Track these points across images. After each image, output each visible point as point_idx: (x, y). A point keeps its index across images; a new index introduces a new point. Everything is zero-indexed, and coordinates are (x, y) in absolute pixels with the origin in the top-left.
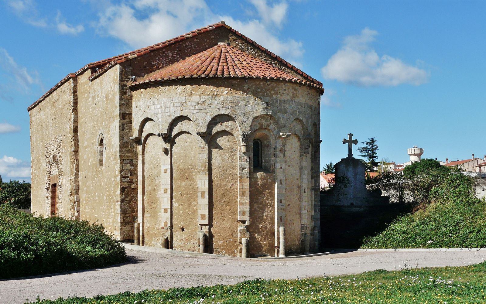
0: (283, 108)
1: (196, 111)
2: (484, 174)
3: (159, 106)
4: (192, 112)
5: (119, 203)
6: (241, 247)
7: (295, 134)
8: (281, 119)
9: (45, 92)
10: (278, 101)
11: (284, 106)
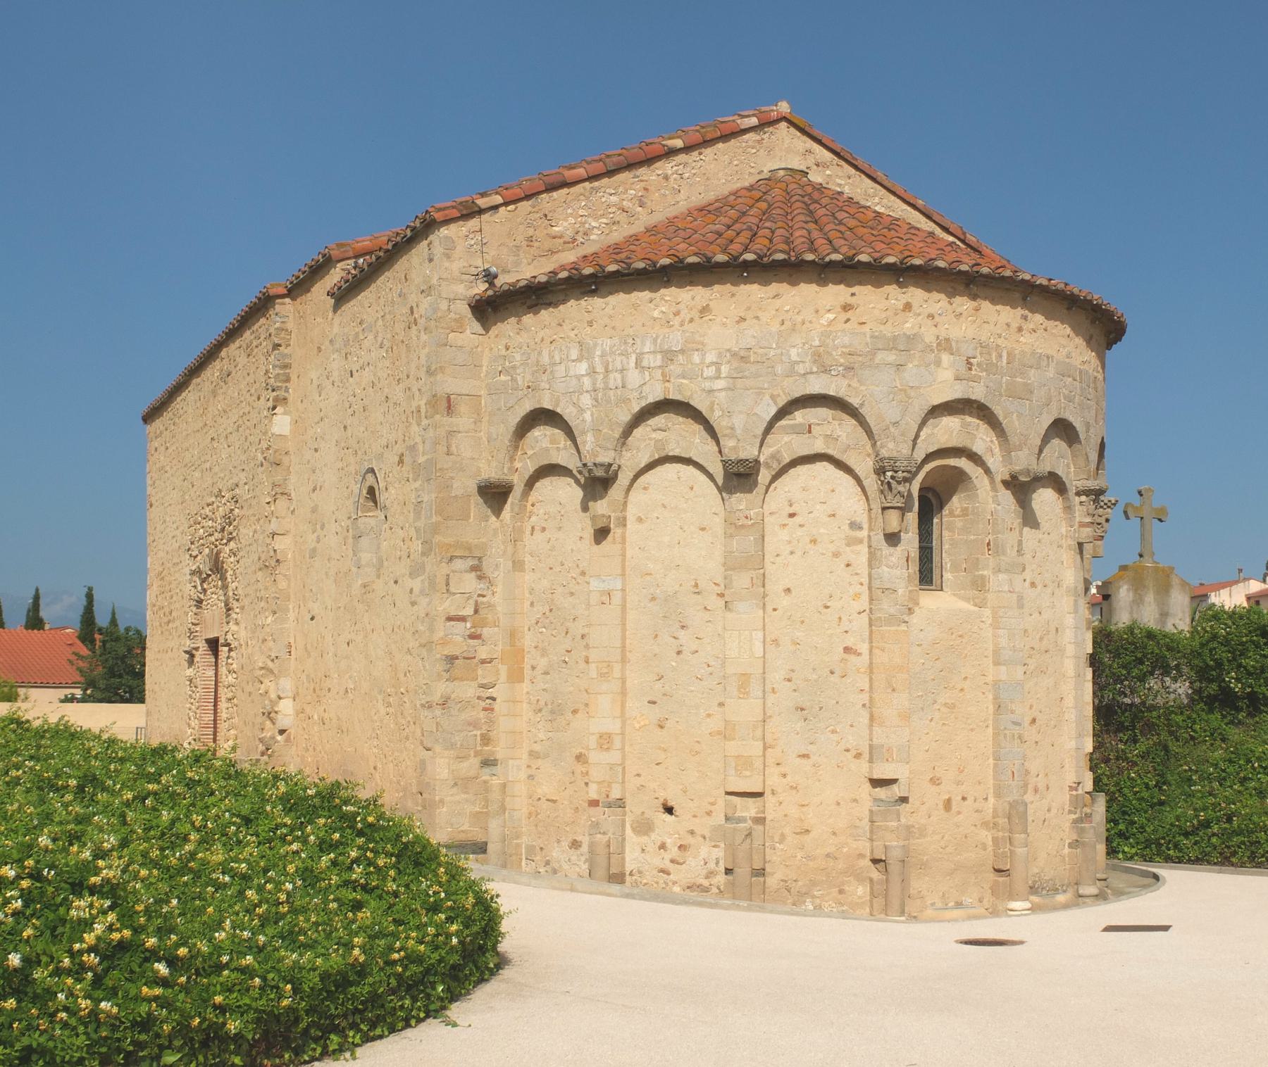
0: (1018, 379)
1: (720, 384)
2: (1267, 631)
3: (583, 368)
4: (707, 385)
9: (190, 359)
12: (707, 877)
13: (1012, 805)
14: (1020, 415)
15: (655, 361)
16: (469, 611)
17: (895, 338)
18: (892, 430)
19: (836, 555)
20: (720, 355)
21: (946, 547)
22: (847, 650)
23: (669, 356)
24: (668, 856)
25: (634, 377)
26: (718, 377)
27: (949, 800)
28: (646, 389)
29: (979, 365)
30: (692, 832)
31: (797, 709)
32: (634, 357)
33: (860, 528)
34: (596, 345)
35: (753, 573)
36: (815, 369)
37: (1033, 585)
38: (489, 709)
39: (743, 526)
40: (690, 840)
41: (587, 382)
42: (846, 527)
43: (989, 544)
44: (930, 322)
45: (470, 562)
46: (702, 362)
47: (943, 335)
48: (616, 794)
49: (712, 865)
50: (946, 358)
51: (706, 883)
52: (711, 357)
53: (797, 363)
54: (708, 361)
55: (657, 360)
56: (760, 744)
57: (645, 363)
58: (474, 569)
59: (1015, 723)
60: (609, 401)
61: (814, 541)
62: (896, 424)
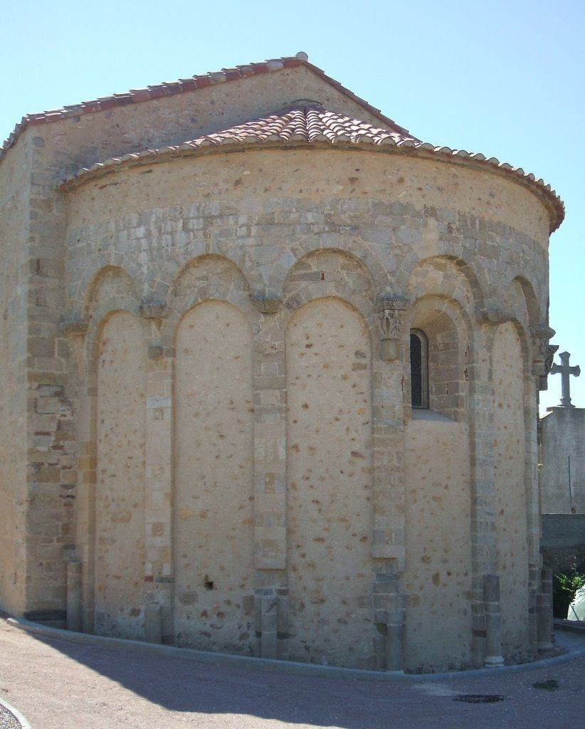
1: (251, 241)
3: (141, 232)
5: (25, 507)
6: (300, 601)
7: (514, 320)
8: (486, 271)
10: (477, 222)
11: (492, 239)
12: (240, 639)
13: (488, 578)
14: (490, 270)
15: (195, 224)
16: (53, 427)
17: (391, 205)
18: (389, 277)
19: (345, 378)
20: (250, 218)
21: (432, 375)
22: (354, 454)
23: (209, 220)
24: (208, 622)
25: (181, 237)
26: (249, 236)
27: (351, 192)
28: (191, 247)
29: (457, 229)
30: (228, 602)
31: (313, 501)
32: (181, 221)
33: (365, 357)
34: (151, 213)
35: (277, 393)
36: (327, 229)
37: (500, 405)
38: (68, 505)
39: (269, 355)
40: (224, 609)
41: (144, 242)
42: (353, 356)
43: (466, 372)
44: (418, 193)
46: (236, 223)
47: (429, 205)
48: (167, 571)
49: (244, 629)
50: (432, 222)
51: (239, 643)
52: (243, 219)
56: (284, 529)
57: (190, 226)
59: (489, 514)
60: (161, 257)
61: (326, 366)
62: (392, 273)
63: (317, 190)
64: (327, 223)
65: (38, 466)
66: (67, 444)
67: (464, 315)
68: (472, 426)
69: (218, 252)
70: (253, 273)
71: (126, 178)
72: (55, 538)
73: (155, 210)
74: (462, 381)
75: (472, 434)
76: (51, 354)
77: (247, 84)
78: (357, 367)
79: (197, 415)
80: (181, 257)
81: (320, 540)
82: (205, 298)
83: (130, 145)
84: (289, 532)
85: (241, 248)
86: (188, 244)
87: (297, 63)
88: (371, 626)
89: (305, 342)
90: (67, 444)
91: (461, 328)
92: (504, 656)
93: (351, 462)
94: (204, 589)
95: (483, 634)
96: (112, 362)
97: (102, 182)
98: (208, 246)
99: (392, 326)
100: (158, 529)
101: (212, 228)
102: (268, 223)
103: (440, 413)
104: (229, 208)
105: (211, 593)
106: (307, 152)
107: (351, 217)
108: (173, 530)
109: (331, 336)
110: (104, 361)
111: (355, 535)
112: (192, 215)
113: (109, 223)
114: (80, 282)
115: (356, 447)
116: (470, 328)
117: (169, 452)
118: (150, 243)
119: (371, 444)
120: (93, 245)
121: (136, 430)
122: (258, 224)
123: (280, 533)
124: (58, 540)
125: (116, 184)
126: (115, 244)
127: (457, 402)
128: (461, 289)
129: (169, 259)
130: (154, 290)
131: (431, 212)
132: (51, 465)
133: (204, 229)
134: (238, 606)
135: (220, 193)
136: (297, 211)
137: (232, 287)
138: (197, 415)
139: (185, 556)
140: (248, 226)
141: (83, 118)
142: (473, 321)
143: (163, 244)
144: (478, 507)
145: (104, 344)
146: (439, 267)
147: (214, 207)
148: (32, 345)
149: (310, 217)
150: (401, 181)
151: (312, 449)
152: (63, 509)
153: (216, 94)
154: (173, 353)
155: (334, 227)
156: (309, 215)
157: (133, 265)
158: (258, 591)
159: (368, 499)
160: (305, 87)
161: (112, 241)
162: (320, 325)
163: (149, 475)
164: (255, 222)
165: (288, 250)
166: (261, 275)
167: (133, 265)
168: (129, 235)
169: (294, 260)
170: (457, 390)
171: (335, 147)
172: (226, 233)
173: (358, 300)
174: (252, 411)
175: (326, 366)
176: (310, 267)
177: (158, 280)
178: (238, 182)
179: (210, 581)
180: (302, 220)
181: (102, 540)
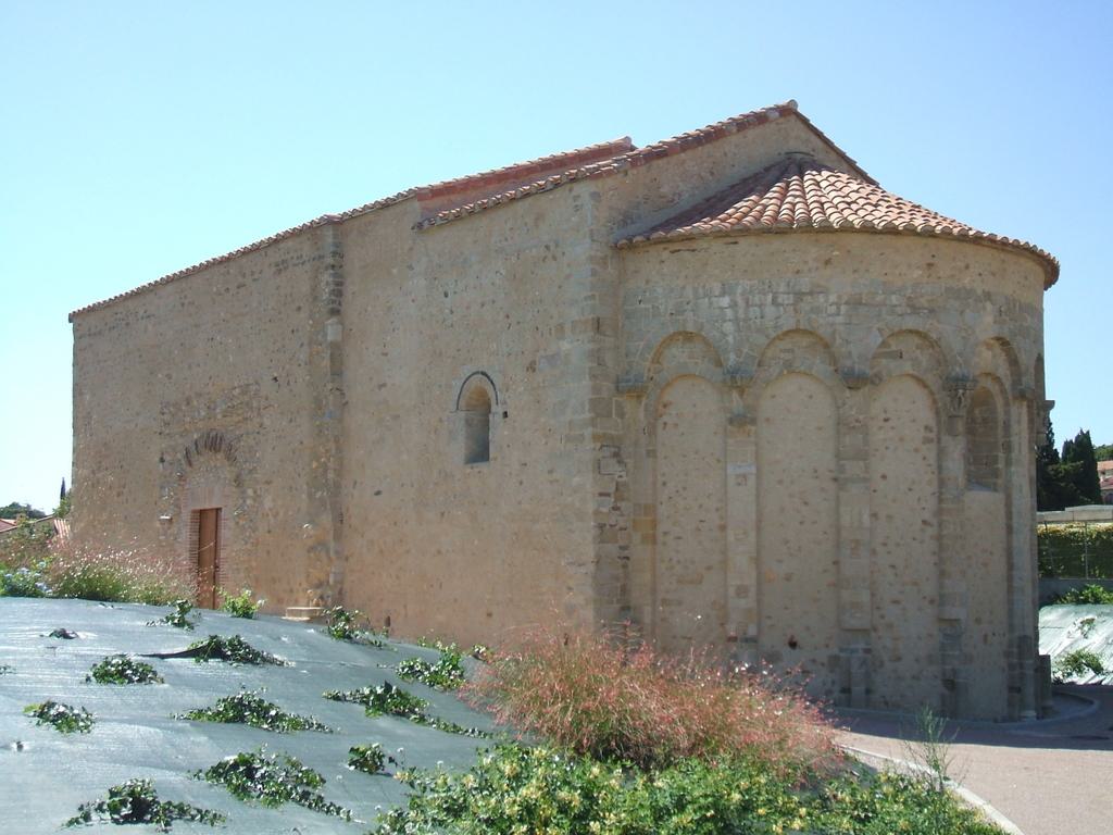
1: (840, 319)
16: (612, 489)
18: (959, 358)
19: (916, 450)
20: (840, 297)
22: (924, 522)
23: (799, 296)
25: (770, 311)
26: (838, 315)
28: (781, 321)
30: (814, 661)
34: (737, 284)
35: (861, 463)
36: (909, 311)
38: (625, 566)
39: (854, 427)
41: (729, 313)
42: (922, 430)
45: (613, 450)
46: (826, 301)
50: (989, 306)
52: (833, 298)
53: (896, 306)
54: (831, 301)
55: (791, 299)
57: (780, 300)
58: (616, 455)
62: (960, 354)
63: (900, 274)
64: (908, 306)
65: (601, 527)
66: (623, 505)
67: (1003, 391)
68: (1008, 497)
69: (808, 328)
70: (844, 349)
71: (705, 245)
72: (615, 600)
73: (741, 282)
74: (1001, 455)
75: (1008, 505)
76: (609, 415)
77: (751, 133)
78: (927, 441)
79: (780, 482)
80: (770, 331)
81: (896, 602)
82: (789, 368)
83: (665, 200)
84: (873, 595)
85: (832, 325)
86: (778, 318)
87: (788, 111)
88: (939, 682)
89: (884, 416)
90: (623, 505)
91: (999, 402)
92: (1036, 710)
93: (922, 530)
94: (789, 649)
95: (1019, 690)
96: (676, 425)
97: (676, 246)
98: (798, 321)
99: (963, 405)
100: (742, 591)
101: (802, 305)
102: (856, 303)
103: (978, 483)
104: (819, 286)
105: (796, 652)
106: (894, 237)
107: (928, 301)
108: (759, 592)
109: (904, 409)
110: (665, 424)
111: (925, 598)
112: (781, 290)
113: (684, 288)
114: (642, 343)
115: (927, 516)
116: (1007, 404)
117: (754, 517)
118: (736, 312)
119: (939, 512)
120: (662, 308)
121: (710, 495)
122: (846, 303)
123: (865, 597)
124: (618, 601)
125: (693, 251)
126: (693, 310)
127: (996, 474)
128: (1003, 370)
129: (759, 331)
130: (741, 360)
131: (988, 296)
132: (611, 526)
133: (794, 304)
134: (823, 664)
135: (810, 270)
136: (883, 293)
137: (818, 361)
138: (780, 482)
139: (769, 617)
140: (838, 305)
141: (629, 172)
142: (1010, 397)
143: (751, 315)
144: (1015, 573)
145: (665, 406)
146: (989, 347)
147: (805, 283)
148: (594, 403)
149: (894, 299)
150: (967, 267)
151: (890, 517)
152: (621, 571)
153: (729, 145)
154: (753, 421)
155: (915, 310)
156: (894, 297)
157: (717, 335)
158: (841, 650)
159: (935, 564)
160: (797, 143)
161: (689, 307)
162: (895, 400)
163: (731, 538)
164: (843, 301)
165: (874, 329)
166: (850, 353)
167: (717, 335)
168: (711, 304)
169: (880, 340)
170: (997, 463)
171: (918, 234)
172: (816, 310)
173: (930, 378)
174: (835, 480)
175: (901, 440)
176: (889, 346)
177: (745, 350)
178: (828, 262)
179: (794, 640)
180: (888, 302)
181: (665, 602)
